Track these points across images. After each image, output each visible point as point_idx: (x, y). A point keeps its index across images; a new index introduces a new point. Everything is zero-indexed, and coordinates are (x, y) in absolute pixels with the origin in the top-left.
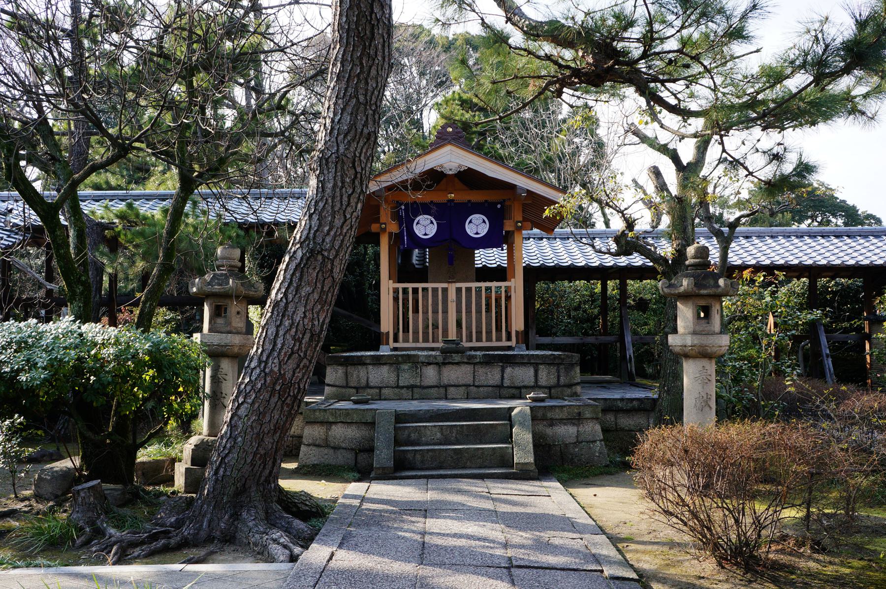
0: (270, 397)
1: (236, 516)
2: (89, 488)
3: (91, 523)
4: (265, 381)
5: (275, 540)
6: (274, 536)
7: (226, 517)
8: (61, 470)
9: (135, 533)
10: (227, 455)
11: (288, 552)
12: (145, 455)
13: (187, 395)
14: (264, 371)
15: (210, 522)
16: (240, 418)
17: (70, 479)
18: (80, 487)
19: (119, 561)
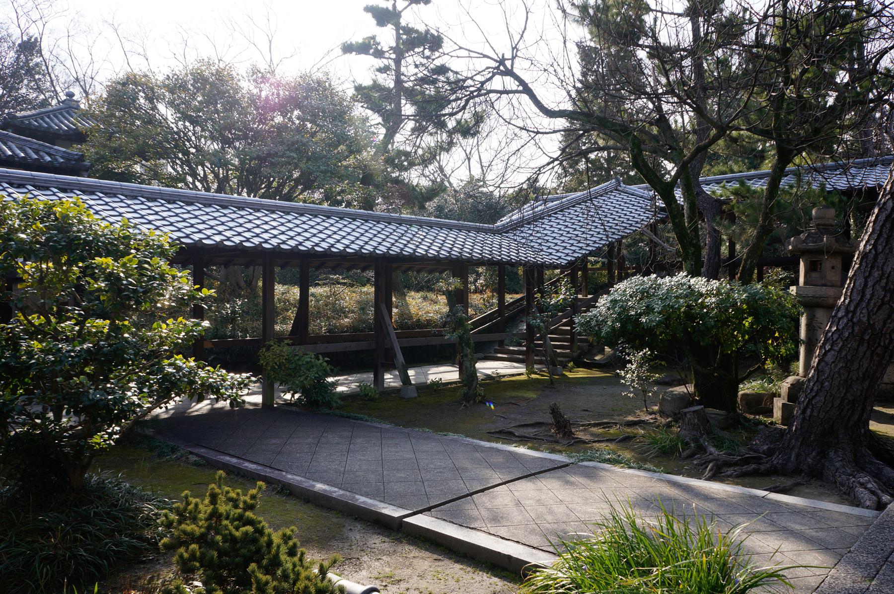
0: (858, 346)
1: (823, 454)
2: (694, 412)
3: (696, 440)
4: (853, 330)
5: (862, 484)
6: (861, 480)
7: (814, 454)
8: (679, 394)
9: (730, 455)
10: (814, 397)
11: (875, 498)
12: (748, 388)
13: (783, 340)
14: (851, 320)
15: (798, 456)
16: (827, 364)
17: (687, 401)
18: (687, 410)
19: (713, 478)
